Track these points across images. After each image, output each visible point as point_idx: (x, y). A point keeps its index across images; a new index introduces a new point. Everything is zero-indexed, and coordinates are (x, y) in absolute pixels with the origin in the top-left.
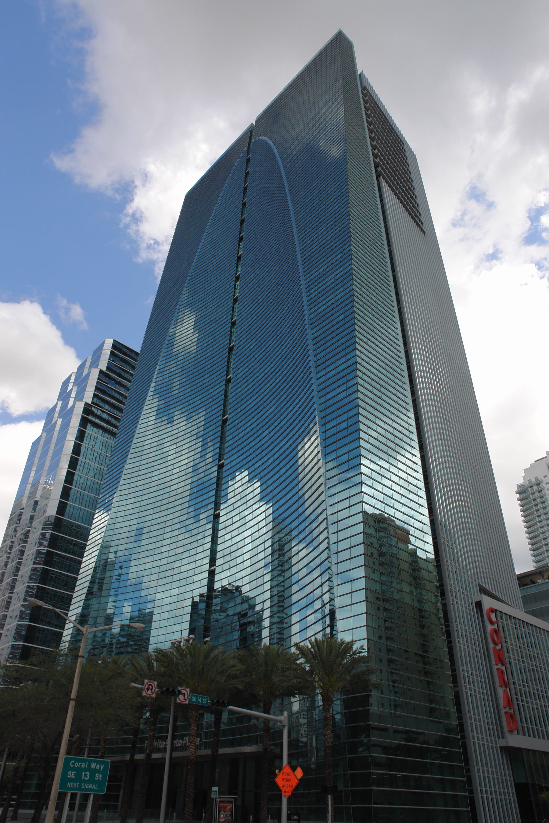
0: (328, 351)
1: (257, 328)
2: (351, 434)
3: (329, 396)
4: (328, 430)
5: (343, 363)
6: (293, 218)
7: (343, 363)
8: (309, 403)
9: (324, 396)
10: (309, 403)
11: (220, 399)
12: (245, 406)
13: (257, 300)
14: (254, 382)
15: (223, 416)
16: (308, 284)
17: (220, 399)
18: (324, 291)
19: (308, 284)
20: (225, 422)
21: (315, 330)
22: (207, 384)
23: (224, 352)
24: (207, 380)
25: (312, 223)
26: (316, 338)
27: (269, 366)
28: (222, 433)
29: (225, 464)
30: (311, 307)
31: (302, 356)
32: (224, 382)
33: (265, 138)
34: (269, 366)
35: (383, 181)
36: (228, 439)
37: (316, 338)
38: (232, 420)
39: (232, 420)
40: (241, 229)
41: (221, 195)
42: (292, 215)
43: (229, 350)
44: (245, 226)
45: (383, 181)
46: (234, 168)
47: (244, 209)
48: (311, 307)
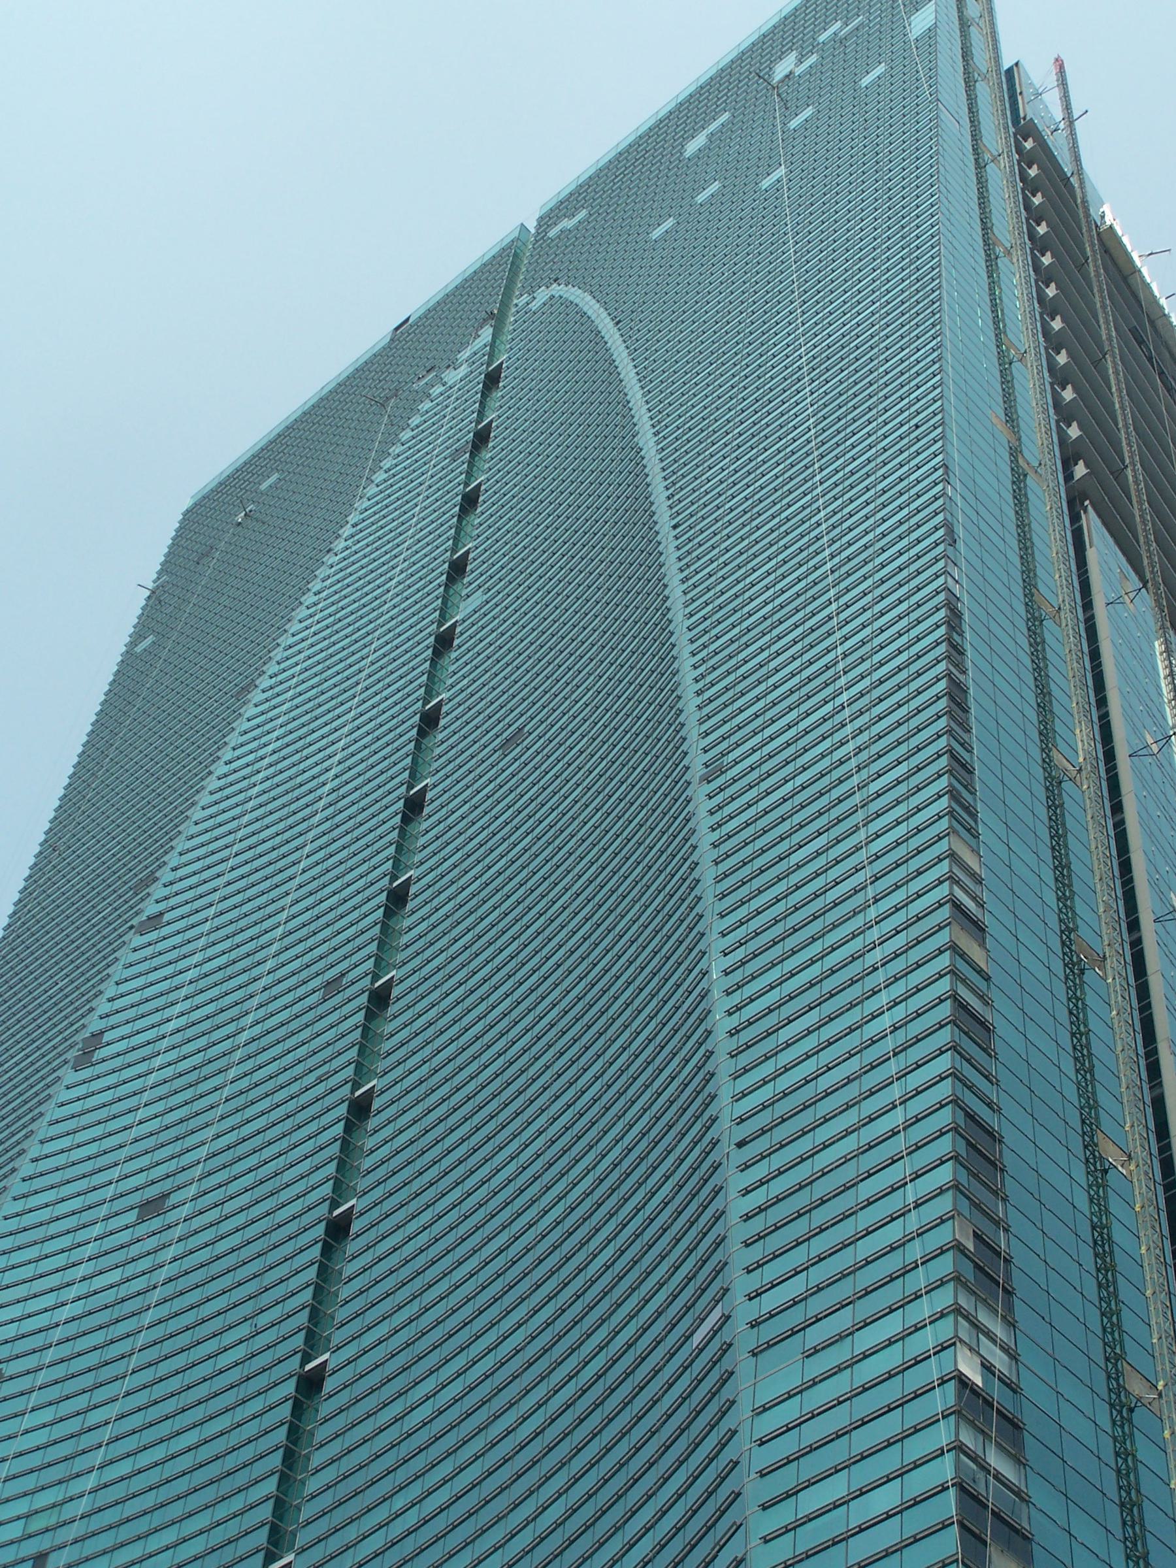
0: (818, 1274)
1: (476, 1120)
2: (916, 1540)
3: (811, 1501)
4: (810, 1519)
5: (890, 1342)
6: (684, 649)
7: (890, 1342)
8: (709, 1528)
9: (788, 1495)
10: (709, 1528)
11: (259, 1469)
12: (396, 1409)
13: (483, 1007)
14: (453, 1300)
15: (307, 1358)
16: (740, 954)
17: (259, 1469)
18: (818, 904)
19: (740, 954)
20: (311, 1384)
21: (760, 1171)
22: (231, 1260)
23: (294, 1284)
24: (235, 1240)
25: (771, 681)
26: (760, 1237)
27: (502, 1489)
28: (294, 1433)
29: (331, 1366)
30: (744, 1060)
31: (695, 1179)
32: (290, 1387)
33: (574, 294)
34: (502, 1489)
35: (1091, 521)
36: (313, 1485)
37: (760, 1237)
38: (346, 1375)
39: (346, 1375)
40: (431, 675)
41: (353, 518)
42: (681, 637)
43: (433, 653)
44: (452, 661)
45: (1091, 521)
46: (427, 405)
47: (458, 587)
48: (744, 1060)
